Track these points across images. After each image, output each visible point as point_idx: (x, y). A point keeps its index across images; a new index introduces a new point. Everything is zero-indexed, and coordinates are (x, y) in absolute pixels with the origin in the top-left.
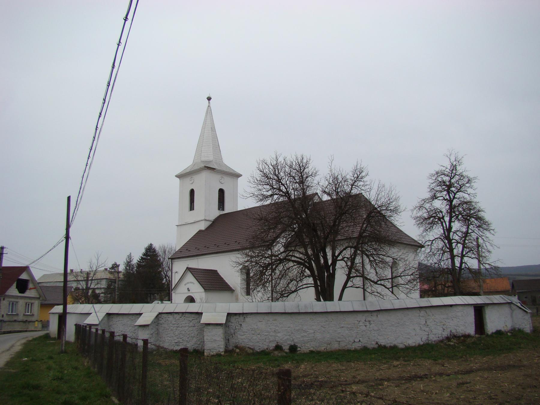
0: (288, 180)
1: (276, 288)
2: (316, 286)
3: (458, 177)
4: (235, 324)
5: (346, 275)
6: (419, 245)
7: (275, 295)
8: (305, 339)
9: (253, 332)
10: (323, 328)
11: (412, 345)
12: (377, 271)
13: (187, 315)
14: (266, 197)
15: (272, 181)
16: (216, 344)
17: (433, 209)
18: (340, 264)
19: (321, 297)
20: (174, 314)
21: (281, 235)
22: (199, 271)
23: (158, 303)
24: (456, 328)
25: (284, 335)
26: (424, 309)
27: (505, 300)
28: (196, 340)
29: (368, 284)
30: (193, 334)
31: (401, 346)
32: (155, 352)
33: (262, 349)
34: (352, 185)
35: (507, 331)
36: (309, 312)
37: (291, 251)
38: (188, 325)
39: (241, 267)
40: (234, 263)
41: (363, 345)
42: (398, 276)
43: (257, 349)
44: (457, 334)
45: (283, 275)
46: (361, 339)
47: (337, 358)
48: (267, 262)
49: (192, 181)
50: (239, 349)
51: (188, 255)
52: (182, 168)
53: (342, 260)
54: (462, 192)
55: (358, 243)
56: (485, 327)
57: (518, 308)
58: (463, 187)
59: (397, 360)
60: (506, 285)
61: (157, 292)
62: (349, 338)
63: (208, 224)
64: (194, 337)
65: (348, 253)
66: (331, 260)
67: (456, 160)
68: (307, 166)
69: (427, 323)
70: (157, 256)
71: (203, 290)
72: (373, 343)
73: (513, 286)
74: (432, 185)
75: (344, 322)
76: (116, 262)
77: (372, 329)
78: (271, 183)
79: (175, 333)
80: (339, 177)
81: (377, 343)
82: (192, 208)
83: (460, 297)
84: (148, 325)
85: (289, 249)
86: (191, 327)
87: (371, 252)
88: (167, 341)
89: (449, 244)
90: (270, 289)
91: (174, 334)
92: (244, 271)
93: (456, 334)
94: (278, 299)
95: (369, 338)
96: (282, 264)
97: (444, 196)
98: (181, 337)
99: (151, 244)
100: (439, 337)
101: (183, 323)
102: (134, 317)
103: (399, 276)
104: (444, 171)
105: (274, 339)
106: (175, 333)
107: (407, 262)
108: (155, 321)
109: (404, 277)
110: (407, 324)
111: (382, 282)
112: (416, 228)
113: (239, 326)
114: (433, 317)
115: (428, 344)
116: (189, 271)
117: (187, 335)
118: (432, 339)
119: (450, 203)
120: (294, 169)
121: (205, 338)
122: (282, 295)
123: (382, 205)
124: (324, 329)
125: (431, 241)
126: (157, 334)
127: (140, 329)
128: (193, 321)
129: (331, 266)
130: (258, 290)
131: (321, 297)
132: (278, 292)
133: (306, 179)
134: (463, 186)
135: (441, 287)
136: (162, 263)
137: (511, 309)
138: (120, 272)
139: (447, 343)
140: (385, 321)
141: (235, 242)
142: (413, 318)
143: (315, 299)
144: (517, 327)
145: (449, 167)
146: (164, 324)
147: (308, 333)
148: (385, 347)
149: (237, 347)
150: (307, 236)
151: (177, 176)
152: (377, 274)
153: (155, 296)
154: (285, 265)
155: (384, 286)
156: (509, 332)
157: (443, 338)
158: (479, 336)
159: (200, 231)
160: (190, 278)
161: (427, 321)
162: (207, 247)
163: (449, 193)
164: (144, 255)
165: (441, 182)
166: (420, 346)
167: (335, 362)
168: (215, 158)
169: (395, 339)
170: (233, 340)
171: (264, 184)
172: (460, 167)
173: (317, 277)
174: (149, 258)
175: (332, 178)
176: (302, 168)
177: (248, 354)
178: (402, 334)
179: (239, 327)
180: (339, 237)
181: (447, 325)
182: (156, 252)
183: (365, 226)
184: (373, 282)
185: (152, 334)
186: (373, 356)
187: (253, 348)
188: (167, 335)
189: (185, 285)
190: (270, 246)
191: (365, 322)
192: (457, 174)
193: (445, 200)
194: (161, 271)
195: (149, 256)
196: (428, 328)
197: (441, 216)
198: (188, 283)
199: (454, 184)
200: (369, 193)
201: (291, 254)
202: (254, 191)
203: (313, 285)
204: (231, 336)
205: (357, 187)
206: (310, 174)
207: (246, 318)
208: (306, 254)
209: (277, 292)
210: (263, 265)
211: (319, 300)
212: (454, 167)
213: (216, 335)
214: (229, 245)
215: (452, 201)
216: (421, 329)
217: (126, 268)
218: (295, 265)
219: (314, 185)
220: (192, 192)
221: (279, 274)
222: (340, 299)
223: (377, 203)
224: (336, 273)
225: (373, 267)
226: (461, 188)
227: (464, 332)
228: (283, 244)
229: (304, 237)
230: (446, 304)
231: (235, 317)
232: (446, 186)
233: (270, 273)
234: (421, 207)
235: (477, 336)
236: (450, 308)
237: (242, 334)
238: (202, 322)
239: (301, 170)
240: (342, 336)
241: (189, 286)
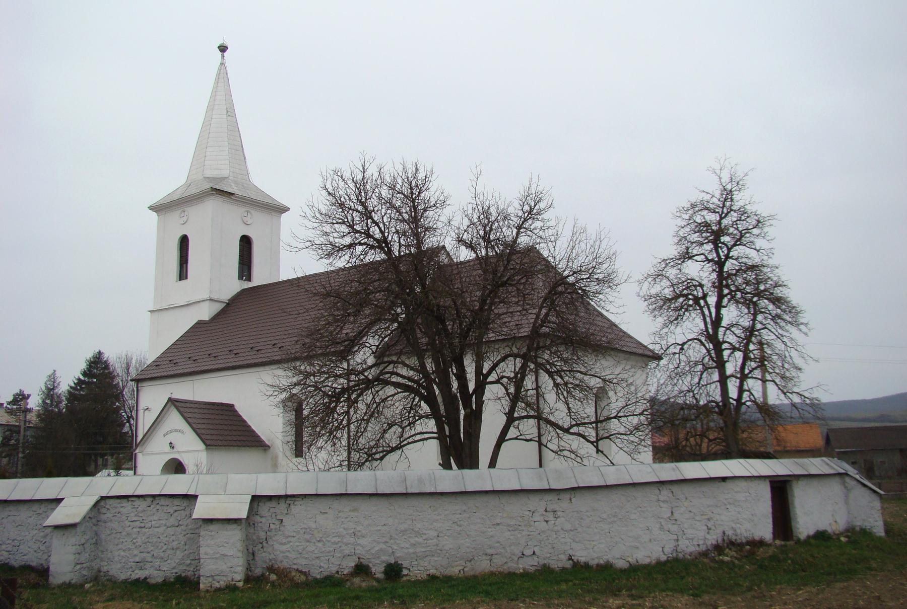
0: (386, 214)
1: (357, 441)
3: (735, 214)
4: (268, 520)
5: (505, 414)
6: (651, 354)
7: (355, 456)
8: (418, 550)
9: (307, 536)
10: (458, 525)
11: (644, 563)
12: (571, 406)
13: (163, 501)
14: (337, 250)
15: (352, 215)
17: (683, 279)
18: (492, 391)
19: (452, 461)
20: (133, 499)
21: (370, 329)
22: (196, 406)
23: (109, 475)
24: (734, 525)
25: (375, 541)
26: (669, 486)
28: (182, 554)
29: (550, 434)
30: (175, 543)
31: (621, 564)
32: (87, 586)
33: (326, 574)
34: (519, 228)
35: (837, 532)
37: (390, 363)
38: (164, 522)
39: (284, 395)
40: (268, 388)
41: (542, 562)
42: (612, 416)
43: (316, 574)
44: (738, 538)
46: (537, 550)
47: (487, 593)
48: (339, 387)
49: (185, 219)
50: (276, 575)
51: (172, 373)
53: (497, 382)
54: (745, 245)
56: (793, 524)
57: (860, 486)
58: (747, 235)
59: (616, 595)
60: (815, 438)
62: (512, 547)
63: (218, 307)
64: (177, 549)
65: (509, 368)
67: (732, 181)
68: (426, 186)
69: (674, 514)
70: (113, 378)
71: (202, 446)
73: (828, 440)
74: (682, 230)
75: (500, 514)
76: (23, 389)
78: (350, 218)
79: (135, 541)
81: (570, 558)
82: (183, 274)
83: (742, 460)
84: (73, 526)
85: (386, 359)
86: (173, 526)
87: (558, 367)
88: (116, 559)
89: (715, 353)
90: (344, 442)
91: (134, 543)
92: (290, 404)
93: (733, 538)
94: (361, 465)
96: (370, 391)
97: (706, 253)
98: (150, 550)
99: (100, 351)
100: (698, 545)
101: (155, 518)
102: (43, 508)
104: (708, 202)
105: (353, 551)
106: (135, 541)
107: (633, 388)
108: (90, 515)
109: (625, 419)
110: (633, 516)
111: (581, 429)
112: (647, 318)
113: (278, 522)
114: (686, 504)
115: (676, 560)
116: (173, 407)
118: (685, 549)
119: (719, 267)
120: (399, 193)
121: (202, 550)
122: (370, 457)
123: (581, 270)
124: (459, 529)
125: (678, 344)
126: (96, 544)
127: (58, 533)
128: (176, 514)
129: (474, 397)
130: (319, 444)
131: (452, 461)
133: (423, 214)
134: (747, 233)
135: (695, 440)
136: (122, 392)
137: (846, 487)
138: (30, 410)
139: (717, 558)
140: (587, 511)
142: (646, 505)
143: (440, 464)
144: (858, 524)
145: (717, 194)
146: (111, 521)
147: (425, 537)
148: (587, 566)
149: (271, 569)
150: (424, 333)
151: (152, 208)
152: (570, 412)
153: (107, 460)
154: (377, 392)
155: (584, 437)
156: (841, 534)
157: (707, 546)
158: (783, 543)
159: (200, 324)
160: (175, 420)
162: (214, 355)
163: (716, 248)
164: (85, 374)
165: (700, 224)
166: (660, 564)
167: (483, 601)
170: (264, 555)
171: (335, 222)
172: (742, 193)
173: (444, 419)
175: (476, 211)
176: (416, 191)
177: (297, 585)
179: (278, 526)
180: (491, 336)
182: (108, 369)
183: (544, 311)
184: (561, 428)
185: (83, 545)
186: (564, 587)
187: (307, 570)
188: (117, 545)
190: (345, 354)
191: (544, 513)
192: (733, 208)
193: (709, 261)
194: (118, 408)
195: (94, 376)
196: (676, 526)
197: (700, 295)
198: (171, 431)
199: (728, 229)
200: (554, 244)
201: (390, 368)
202: (313, 236)
204: (261, 545)
206: (432, 204)
207: (292, 506)
208: (422, 369)
209: (358, 451)
210: (330, 393)
211: (449, 467)
212: (727, 194)
214: (259, 352)
215: (724, 263)
216: (661, 528)
217: (44, 402)
218: (398, 393)
219: (440, 225)
220: (184, 242)
221: (365, 411)
222: (492, 464)
223: (570, 264)
224: (484, 409)
225: (561, 397)
226: (742, 236)
227: (751, 536)
228: (374, 348)
229: (419, 335)
230: (712, 476)
232: (713, 232)
233: (345, 409)
234: (659, 275)
235: (778, 542)
236: (723, 483)
237: (284, 541)
238: (194, 516)
239: (412, 193)
240: (498, 542)
241: (171, 437)
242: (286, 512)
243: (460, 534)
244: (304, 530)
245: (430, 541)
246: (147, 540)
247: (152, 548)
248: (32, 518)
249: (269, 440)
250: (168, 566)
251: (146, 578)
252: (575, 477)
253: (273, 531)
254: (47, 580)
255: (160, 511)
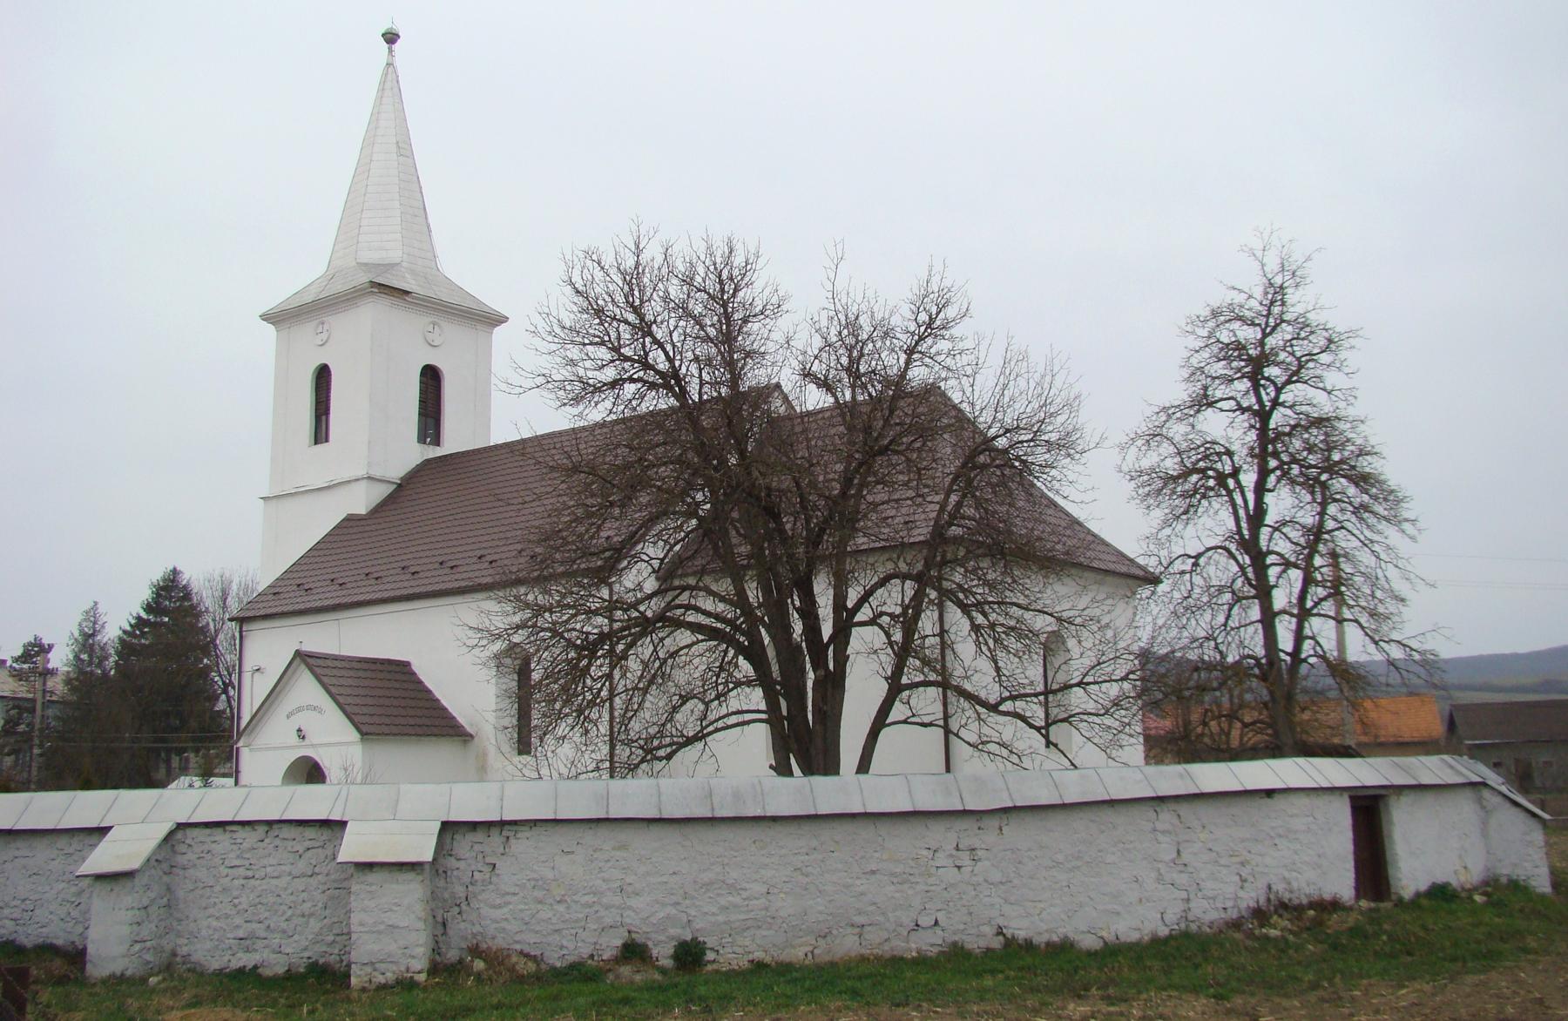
2: (773, 717)
3: (1290, 328)
4: (470, 865)
5: (886, 679)
6: (1141, 573)
7: (622, 753)
8: (733, 917)
9: (539, 894)
10: (803, 874)
11: (1129, 940)
12: (1001, 664)
13: (286, 832)
14: (591, 390)
15: (617, 329)
16: (395, 941)
17: (1198, 443)
18: (863, 639)
20: (234, 828)
23: (191, 786)
24: (1286, 874)
25: (657, 901)
26: (1173, 806)
27: (1460, 774)
28: (319, 925)
30: (308, 905)
31: (1089, 942)
33: (571, 959)
36: (752, 815)
37: (683, 589)
38: (287, 868)
39: (498, 646)
42: (1073, 682)
43: (555, 959)
44: (1293, 896)
45: (654, 676)
46: (941, 916)
47: (855, 993)
48: (595, 631)
49: (324, 336)
50: (485, 960)
52: (284, 288)
53: (872, 622)
54: (1306, 382)
55: (928, 566)
56: (1391, 871)
57: (1508, 805)
58: (1311, 365)
59: (1080, 997)
60: (1430, 721)
61: (191, 744)
62: (898, 913)
64: (311, 915)
65: (893, 598)
66: (830, 622)
68: (746, 279)
69: (1183, 855)
70: (198, 615)
72: (988, 930)
73: (1451, 725)
74: (1196, 355)
75: (877, 855)
77: (981, 879)
78: (613, 335)
80: (864, 321)
81: (1000, 932)
82: (321, 433)
83: (1301, 760)
85: (677, 583)
86: (303, 875)
87: (979, 597)
88: (204, 932)
90: (604, 728)
91: (235, 906)
92: (508, 661)
93: (1286, 897)
94: (632, 769)
95: (971, 914)
96: (649, 639)
98: (262, 917)
99: (175, 569)
100: (1225, 909)
102: (76, 843)
103: (1079, 685)
104: (1242, 306)
105: (619, 919)
106: (236, 901)
107: (1110, 633)
109: (1096, 687)
111: (1020, 705)
112: (1135, 511)
113: (487, 869)
114: (1203, 836)
115: (1186, 935)
116: (303, 666)
117: (284, 907)
118: (1201, 915)
120: (699, 290)
121: (355, 918)
122: (650, 754)
125: (1190, 557)
126: (168, 906)
127: (104, 888)
128: (309, 853)
129: (831, 648)
132: (633, 742)
133: (741, 327)
134: (1309, 360)
136: (213, 640)
137: (1483, 807)
138: (53, 672)
139: (1257, 932)
140: (1030, 850)
141: (480, 558)
143: (771, 767)
145: (1258, 292)
146: (195, 866)
147: (745, 895)
148: (1029, 946)
149: (475, 951)
150: (745, 537)
151: (266, 317)
152: (999, 676)
153: (187, 760)
154: (662, 640)
155: (1023, 719)
156: (1475, 889)
158: (1373, 905)
159: (350, 520)
160: (307, 689)
161: (1181, 849)
162: (376, 575)
163: (1256, 387)
164: (149, 608)
165: (1228, 345)
166: (1156, 941)
167: (847, 1008)
168: (409, 255)
169: (1063, 916)
170: (462, 925)
171: (587, 341)
172: (1301, 290)
173: (778, 687)
174: (167, 619)
175: (835, 323)
176: (729, 288)
177: (521, 979)
178: (1091, 899)
179: (488, 876)
180: (861, 541)
181: (1254, 863)
183: (954, 498)
184: (984, 704)
185: (145, 908)
186: (988, 982)
187: (538, 953)
189: (288, 717)
190: (605, 573)
191: (954, 852)
192: (1286, 317)
193: (1243, 410)
194: (208, 669)
195: (165, 612)
197: (1228, 469)
198: (300, 709)
199: (1277, 355)
201: (684, 598)
203: (764, 716)
204: (457, 910)
205: (927, 360)
206: (757, 310)
207: (512, 840)
208: (740, 601)
209: (629, 743)
210: (579, 642)
212: (1275, 293)
213: (395, 908)
215: (1269, 415)
216: (1160, 879)
217: (77, 657)
218: (698, 641)
219: (771, 347)
220: (323, 376)
221: (639, 673)
222: (864, 766)
224: (848, 670)
225: (984, 648)
226: (1300, 367)
228: (656, 564)
229: (734, 541)
230: (1250, 787)
231: (471, 837)
232: (1250, 359)
233: (605, 669)
234: (1155, 436)
235: (1364, 904)
237: (498, 901)
239: (722, 291)
241: (301, 720)
242: (502, 850)
243: (806, 889)
244: (533, 883)
245: (755, 902)
246: (257, 900)
247: (267, 914)
248: (57, 861)
249: (472, 725)
250: (294, 945)
251: (256, 967)
252: (1008, 789)
253: (479, 883)
254: (83, 969)
255: (280, 850)
